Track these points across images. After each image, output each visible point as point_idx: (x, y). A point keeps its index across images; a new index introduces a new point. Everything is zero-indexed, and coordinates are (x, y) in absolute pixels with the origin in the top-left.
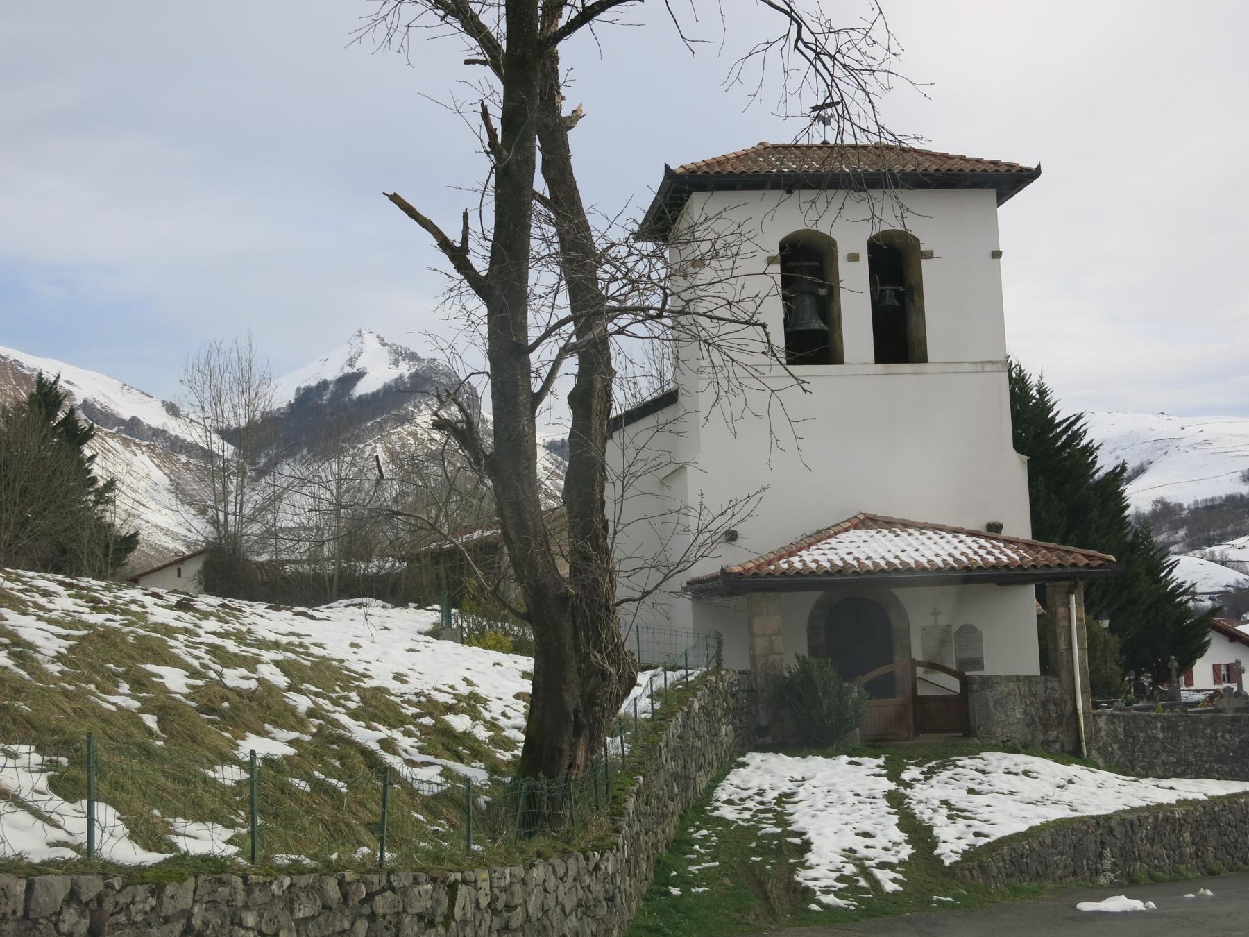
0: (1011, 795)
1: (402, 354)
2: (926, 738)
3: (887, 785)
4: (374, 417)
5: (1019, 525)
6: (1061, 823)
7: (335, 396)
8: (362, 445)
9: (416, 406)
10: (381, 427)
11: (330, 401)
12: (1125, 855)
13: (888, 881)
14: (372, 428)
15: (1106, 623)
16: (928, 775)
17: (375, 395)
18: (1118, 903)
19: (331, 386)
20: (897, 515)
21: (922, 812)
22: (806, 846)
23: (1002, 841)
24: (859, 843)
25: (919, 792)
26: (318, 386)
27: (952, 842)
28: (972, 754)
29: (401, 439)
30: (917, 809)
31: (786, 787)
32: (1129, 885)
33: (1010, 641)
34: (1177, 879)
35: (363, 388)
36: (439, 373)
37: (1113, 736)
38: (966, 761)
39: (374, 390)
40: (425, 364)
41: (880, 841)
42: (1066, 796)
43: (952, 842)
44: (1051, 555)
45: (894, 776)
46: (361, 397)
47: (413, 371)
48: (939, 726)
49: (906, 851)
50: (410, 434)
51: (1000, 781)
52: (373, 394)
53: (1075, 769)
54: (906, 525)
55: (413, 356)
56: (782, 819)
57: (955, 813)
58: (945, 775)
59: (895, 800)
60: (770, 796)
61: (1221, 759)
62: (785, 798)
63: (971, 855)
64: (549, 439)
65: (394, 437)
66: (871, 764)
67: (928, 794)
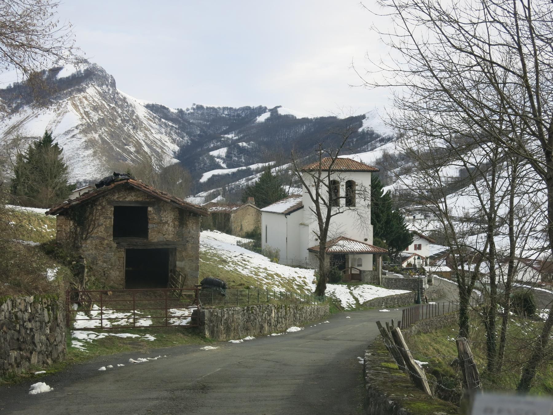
0: (369, 292)
1: (79, 61)
2: (353, 281)
3: (349, 291)
4: (68, 88)
5: (370, 242)
6: (377, 298)
7: (49, 78)
8: (61, 101)
9: (87, 85)
10: (70, 93)
11: (47, 79)
12: (386, 303)
13: (354, 306)
14: (66, 94)
15: (385, 241)
16: (355, 288)
17: (68, 78)
18: (385, 310)
19: (47, 72)
20: (348, 237)
21: (356, 296)
22: (340, 301)
23: (368, 301)
24: (348, 301)
25: (354, 292)
26: (41, 72)
27: (361, 301)
28: (361, 285)
29: (79, 99)
30: (355, 295)
31: (333, 291)
32: (386, 308)
33: (367, 265)
34: (394, 307)
35: (62, 75)
36: (97, 70)
37: (385, 281)
38: (360, 286)
39: (67, 76)
40: (91, 65)
41: (351, 300)
42: (378, 293)
43: (361, 301)
44: (376, 250)
45: (349, 289)
46: (61, 79)
47: (86, 68)
48: (356, 280)
49: (355, 302)
50: (84, 97)
51: (366, 290)
52: (67, 78)
53: (379, 288)
54: (350, 240)
55: (86, 61)
56: (335, 296)
57: (361, 296)
58: (358, 289)
59: (351, 293)
60: (331, 292)
61: (404, 286)
62: (333, 292)
63: (364, 303)
64: (146, 103)
65: (76, 98)
66: (345, 286)
67: (357, 292)
